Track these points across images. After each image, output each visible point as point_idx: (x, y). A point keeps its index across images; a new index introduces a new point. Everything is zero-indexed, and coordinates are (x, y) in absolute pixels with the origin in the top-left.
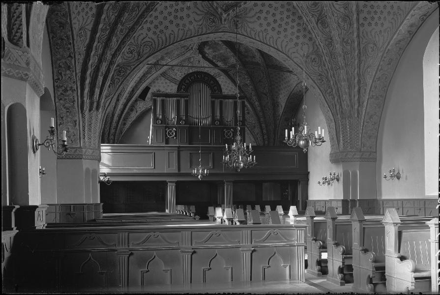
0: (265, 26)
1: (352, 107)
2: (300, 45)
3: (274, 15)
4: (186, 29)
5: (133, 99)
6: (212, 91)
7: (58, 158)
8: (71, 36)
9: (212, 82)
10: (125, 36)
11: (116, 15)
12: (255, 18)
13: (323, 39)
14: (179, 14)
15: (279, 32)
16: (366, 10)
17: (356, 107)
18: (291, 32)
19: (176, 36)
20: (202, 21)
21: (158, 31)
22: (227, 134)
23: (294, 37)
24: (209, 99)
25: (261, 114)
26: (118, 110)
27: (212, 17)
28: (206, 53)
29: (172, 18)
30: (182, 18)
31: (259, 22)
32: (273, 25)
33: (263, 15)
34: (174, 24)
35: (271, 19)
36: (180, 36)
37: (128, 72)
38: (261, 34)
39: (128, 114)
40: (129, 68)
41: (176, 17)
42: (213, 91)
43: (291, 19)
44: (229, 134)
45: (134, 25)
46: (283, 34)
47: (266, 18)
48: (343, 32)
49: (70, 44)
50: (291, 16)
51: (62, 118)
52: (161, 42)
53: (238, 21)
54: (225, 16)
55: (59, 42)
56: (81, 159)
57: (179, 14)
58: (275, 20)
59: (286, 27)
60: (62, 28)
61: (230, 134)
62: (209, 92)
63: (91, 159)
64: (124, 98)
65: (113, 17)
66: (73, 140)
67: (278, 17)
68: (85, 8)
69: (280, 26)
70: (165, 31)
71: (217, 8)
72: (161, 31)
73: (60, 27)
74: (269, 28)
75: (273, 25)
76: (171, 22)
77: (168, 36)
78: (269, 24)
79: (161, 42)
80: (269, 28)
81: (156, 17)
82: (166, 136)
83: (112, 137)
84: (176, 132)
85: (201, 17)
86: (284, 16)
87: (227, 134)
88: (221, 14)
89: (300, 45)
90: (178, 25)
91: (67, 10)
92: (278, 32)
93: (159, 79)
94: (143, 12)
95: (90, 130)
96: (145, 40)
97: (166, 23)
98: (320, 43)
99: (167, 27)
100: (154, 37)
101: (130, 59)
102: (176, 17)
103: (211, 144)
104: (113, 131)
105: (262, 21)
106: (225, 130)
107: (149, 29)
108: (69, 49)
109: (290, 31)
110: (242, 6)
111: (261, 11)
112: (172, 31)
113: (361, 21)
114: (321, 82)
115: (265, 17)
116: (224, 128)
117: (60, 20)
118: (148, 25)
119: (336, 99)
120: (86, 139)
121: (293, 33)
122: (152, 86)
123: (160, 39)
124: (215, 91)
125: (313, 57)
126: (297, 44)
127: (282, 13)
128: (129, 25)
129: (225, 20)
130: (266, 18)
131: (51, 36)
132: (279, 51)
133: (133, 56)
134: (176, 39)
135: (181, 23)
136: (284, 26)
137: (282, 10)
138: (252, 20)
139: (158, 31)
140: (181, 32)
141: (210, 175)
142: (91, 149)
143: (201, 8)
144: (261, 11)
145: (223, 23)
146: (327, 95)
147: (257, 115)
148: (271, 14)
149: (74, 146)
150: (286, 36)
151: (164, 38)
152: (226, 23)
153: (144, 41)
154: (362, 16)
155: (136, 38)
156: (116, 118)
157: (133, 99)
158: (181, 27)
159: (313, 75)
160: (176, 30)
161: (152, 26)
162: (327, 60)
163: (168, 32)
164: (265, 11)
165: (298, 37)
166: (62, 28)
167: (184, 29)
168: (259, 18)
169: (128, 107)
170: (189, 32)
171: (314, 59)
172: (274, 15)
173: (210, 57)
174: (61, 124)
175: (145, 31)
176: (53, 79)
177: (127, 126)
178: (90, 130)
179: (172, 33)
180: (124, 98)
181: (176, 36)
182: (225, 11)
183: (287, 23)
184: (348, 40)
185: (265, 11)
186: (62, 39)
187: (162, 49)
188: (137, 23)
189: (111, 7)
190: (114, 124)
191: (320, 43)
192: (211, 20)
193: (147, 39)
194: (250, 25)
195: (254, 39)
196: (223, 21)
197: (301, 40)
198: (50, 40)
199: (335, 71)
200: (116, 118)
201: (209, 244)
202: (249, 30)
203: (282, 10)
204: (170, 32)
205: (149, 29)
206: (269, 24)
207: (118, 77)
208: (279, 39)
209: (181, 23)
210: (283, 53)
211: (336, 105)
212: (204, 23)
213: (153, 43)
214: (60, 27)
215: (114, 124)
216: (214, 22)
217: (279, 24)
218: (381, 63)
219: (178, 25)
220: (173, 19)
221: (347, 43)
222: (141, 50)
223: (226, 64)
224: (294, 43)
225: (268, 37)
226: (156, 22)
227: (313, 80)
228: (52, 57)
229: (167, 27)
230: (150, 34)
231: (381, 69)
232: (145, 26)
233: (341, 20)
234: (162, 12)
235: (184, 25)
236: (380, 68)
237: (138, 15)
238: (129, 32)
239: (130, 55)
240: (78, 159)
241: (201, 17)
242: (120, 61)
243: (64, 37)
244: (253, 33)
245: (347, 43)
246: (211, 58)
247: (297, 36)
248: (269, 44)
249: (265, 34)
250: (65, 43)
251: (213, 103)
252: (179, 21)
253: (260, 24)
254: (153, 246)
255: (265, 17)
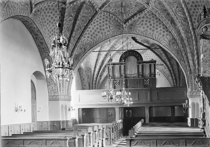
0: (146, 28)
1: (195, 67)
2: (165, 36)
3: (150, 22)
4: (106, 34)
5: (104, 66)
6: (138, 60)
7: (49, 101)
8: (47, 47)
9: (137, 55)
10: (76, 42)
11: (70, 33)
12: (140, 25)
13: (176, 32)
14: (102, 28)
15: (153, 30)
16: (194, 15)
17: (197, 67)
18: (160, 30)
19: (102, 38)
20: (114, 30)
21: (93, 37)
22: (146, 82)
23: (162, 32)
24: (136, 64)
25: (171, 69)
26: (96, 72)
27: (119, 27)
28: (137, 39)
29: (99, 30)
30: (104, 30)
31: (142, 26)
32: (150, 27)
33: (144, 23)
34: (100, 33)
35: (148, 24)
36: (104, 38)
37: (80, 58)
38: (144, 32)
39: (102, 73)
40: (80, 56)
41: (101, 29)
42: (138, 60)
43: (158, 23)
44: (147, 82)
45: (80, 37)
46: (156, 31)
47: (146, 24)
48: (185, 27)
49: (47, 50)
50: (158, 21)
51: (49, 82)
52: (94, 42)
53: (132, 27)
54: (124, 25)
55: (43, 50)
56: (59, 100)
57: (102, 28)
58: (150, 24)
59: (157, 27)
60: (42, 44)
61: (148, 82)
62: (136, 60)
63: (64, 100)
64: (98, 66)
65: (69, 34)
66: (55, 92)
67: (152, 22)
68: (49, 33)
69: (154, 27)
70: (96, 37)
71: (120, 22)
72: (95, 37)
73: (41, 44)
74: (148, 29)
75: (150, 27)
76: (99, 32)
77: (98, 39)
78: (148, 27)
79: (94, 42)
80: (148, 29)
81: (91, 31)
82: (114, 85)
83: (94, 85)
84: (119, 82)
85: (113, 28)
86: (155, 22)
87: (146, 82)
88: (123, 25)
89: (165, 36)
90: (102, 33)
91: (42, 37)
92: (153, 30)
93: (116, 54)
94: (83, 30)
95: (63, 86)
96: (87, 42)
97: (96, 33)
98: (174, 34)
99: (97, 35)
100: (92, 40)
101: (81, 52)
102: (101, 29)
103: (137, 88)
104: (94, 82)
105: (144, 25)
106: (145, 80)
107: (88, 37)
108: (47, 52)
109: (159, 29)
110: (133, 20)
111: (143, 21)
112: (100, 36)
113: (193, 20)
114: (178, 55)
115: (145, 24)
116: (144, 79)
117: (40, 41)
118: (88, 35)
119: (186, 63)
120: (61, 91)
121: (161, 30)
122: (113, 58)
123: (94, 41)
124: (139, 59)
125: (173, 41)
126: (163, 35)
127: (153, 20)
128: (78, 36)
129: (125, 28)
130: (146, 24)
131: (39, 48)
132: (154, 40)
133: (82, 50)
134: (101, 40)
135: (103, 32)
136: (156, 27)
137: (153, 19)
138: (139, 26)
139: (93, 37)
140: (104, 36)
141: (133, 104)
142: (64, 96)
143: (113, 24)
144: (143, 21)
145: (124, 29)
146: (182, 61)
147: (169, 69)
148: (148, 21)
149: (55, 95)
150: (157, 32)
151: (96, 40)
152: (126, 29)
153: (86, 43)
154: (193, 18)
155: (82, 42)
156: (95, 76)
157: (104, 66)
158: (104, 34)
159: (173, 51)
160: (101, 35)
161: (90, 35)
162: (179, 43)
163: (98, 37)
164: (145, 20)
165: (164, 32)
166: (42, 44)
167: (105, 34)
168: (142, 24)
169: (101, 70)
170: (100, 39)
171: (174, 42)
172: (150, 22)
173: (140, 41)
174: (49, 85)
175: (86, 38)
176: (44, 66)
177: (103, 78)
178: (63, 86)
179: (100, 37)
180: (98, 66)
181: (102, 38)
182: (125, 23)
183: (157, 25)
184: (188, 31)
185: (145, 20)
186: (44, 49)
187: (95, 46)
188: (81, 35)
189: (66, 31)
190: (95, 79)
191: (174, 34)
192: (118, 28)
193: (88, 42)
194: (138, 28)
195: (140, 35)
196: (124, 28)
197: (166, 33)
198: (39, 50)
199: (185, 48)
200: (95, 76)
201: (30, 145)
202: (138, 31)
203: (153, 19)
204: (99, 37)
205: (88, 37)
206: (148, 27)
207: (76, 61)
208: (154, 34)
209: (103, 32)
210: (157, 41)
211: (186, 67)
212: (115, 30)
213: (91, 44)
214: (41, 44)
215: (95, 79)
216: (120, 29)
217: (153, 26)
218: (204, 43)
219: (102, 33)
220: (99, 30)
221: (188, 32)
222: (86, 47)
223: (149, 44)
224: (162, 35)
225: (148, 34)
226: (91, 33)
227: (173, 54)
228: (41, 57)
229: (97, 35)
230: (89, 39)
231: (205, 46)
232: (86, 36)
233: (182, 21)
234: (93, 28)
235: (105, 33)
236: (204, 45)
237: (81, 32)
238: (78, 40)
239: (81, 50)
240: (57, 100)
241: (113, 28)
242: (76, 53)
243: (44, 48)
244: (140, 32)
245: (188, 32)
246: (141, 42)
247: (163, 31)
248: (147, 36)
249: (146, 32)
250: (45, 50)
251: (138, 66)
252: (102, 31)
253: (143, 27)
254: (12, 145)
255: (145, 24)
